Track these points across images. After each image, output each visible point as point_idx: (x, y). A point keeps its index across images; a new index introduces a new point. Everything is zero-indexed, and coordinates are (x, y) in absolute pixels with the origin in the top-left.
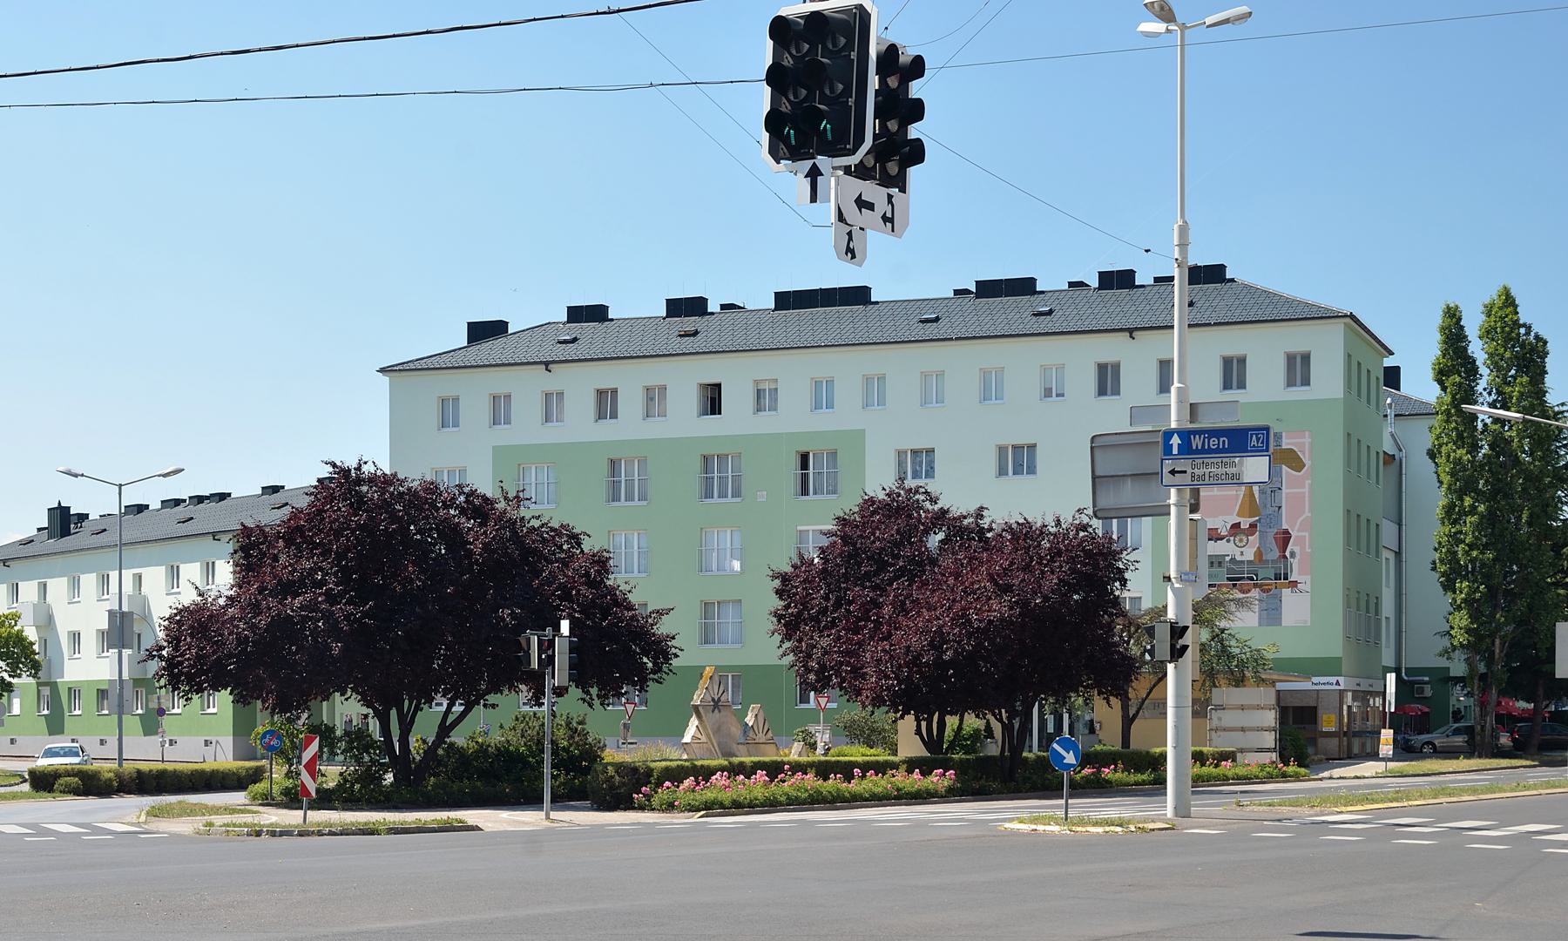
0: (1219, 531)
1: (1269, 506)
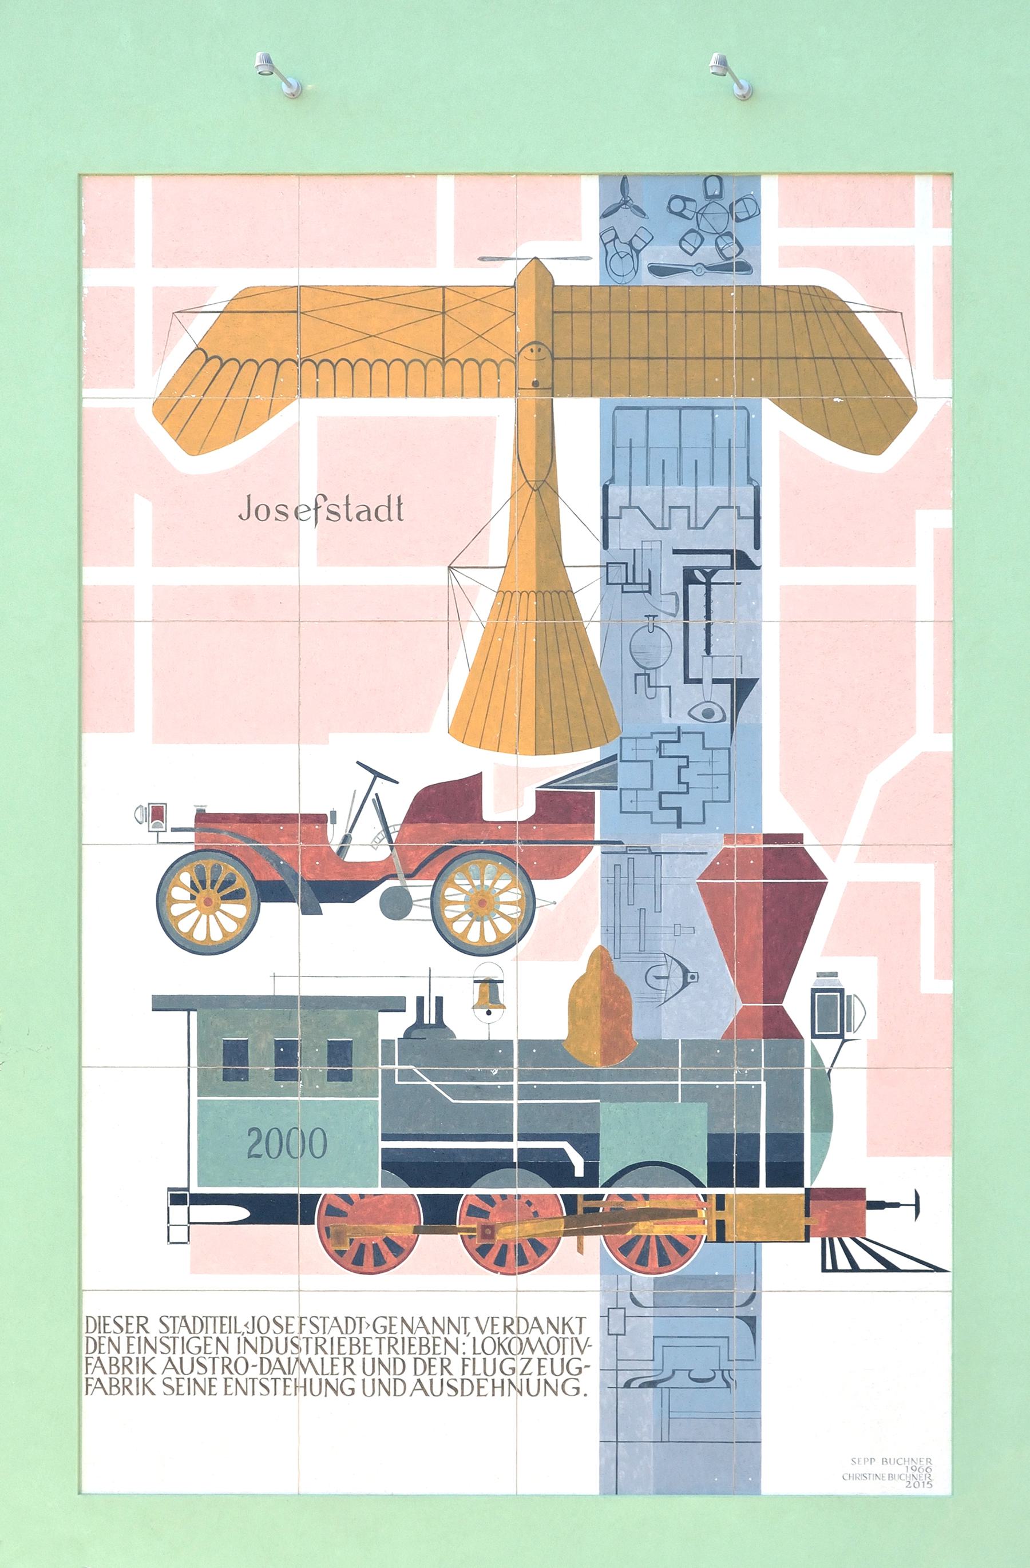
0: (335, 835)
1: (671, 673)
